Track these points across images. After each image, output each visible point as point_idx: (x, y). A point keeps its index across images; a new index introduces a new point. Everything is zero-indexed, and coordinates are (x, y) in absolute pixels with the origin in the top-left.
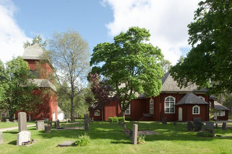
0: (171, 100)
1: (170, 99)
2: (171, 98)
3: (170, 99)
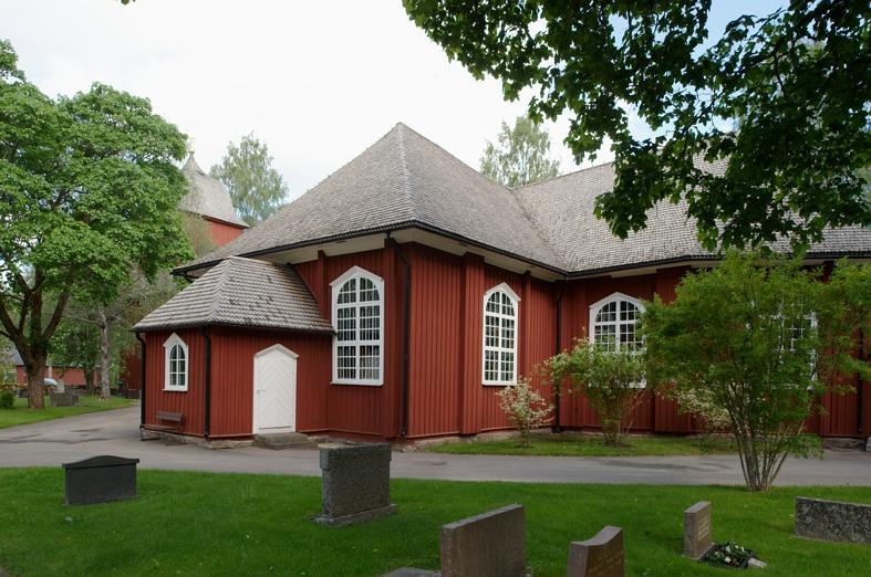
0: (623, 317)
1: (618, 312)
2: (623, 305)
3: (618, 312)
